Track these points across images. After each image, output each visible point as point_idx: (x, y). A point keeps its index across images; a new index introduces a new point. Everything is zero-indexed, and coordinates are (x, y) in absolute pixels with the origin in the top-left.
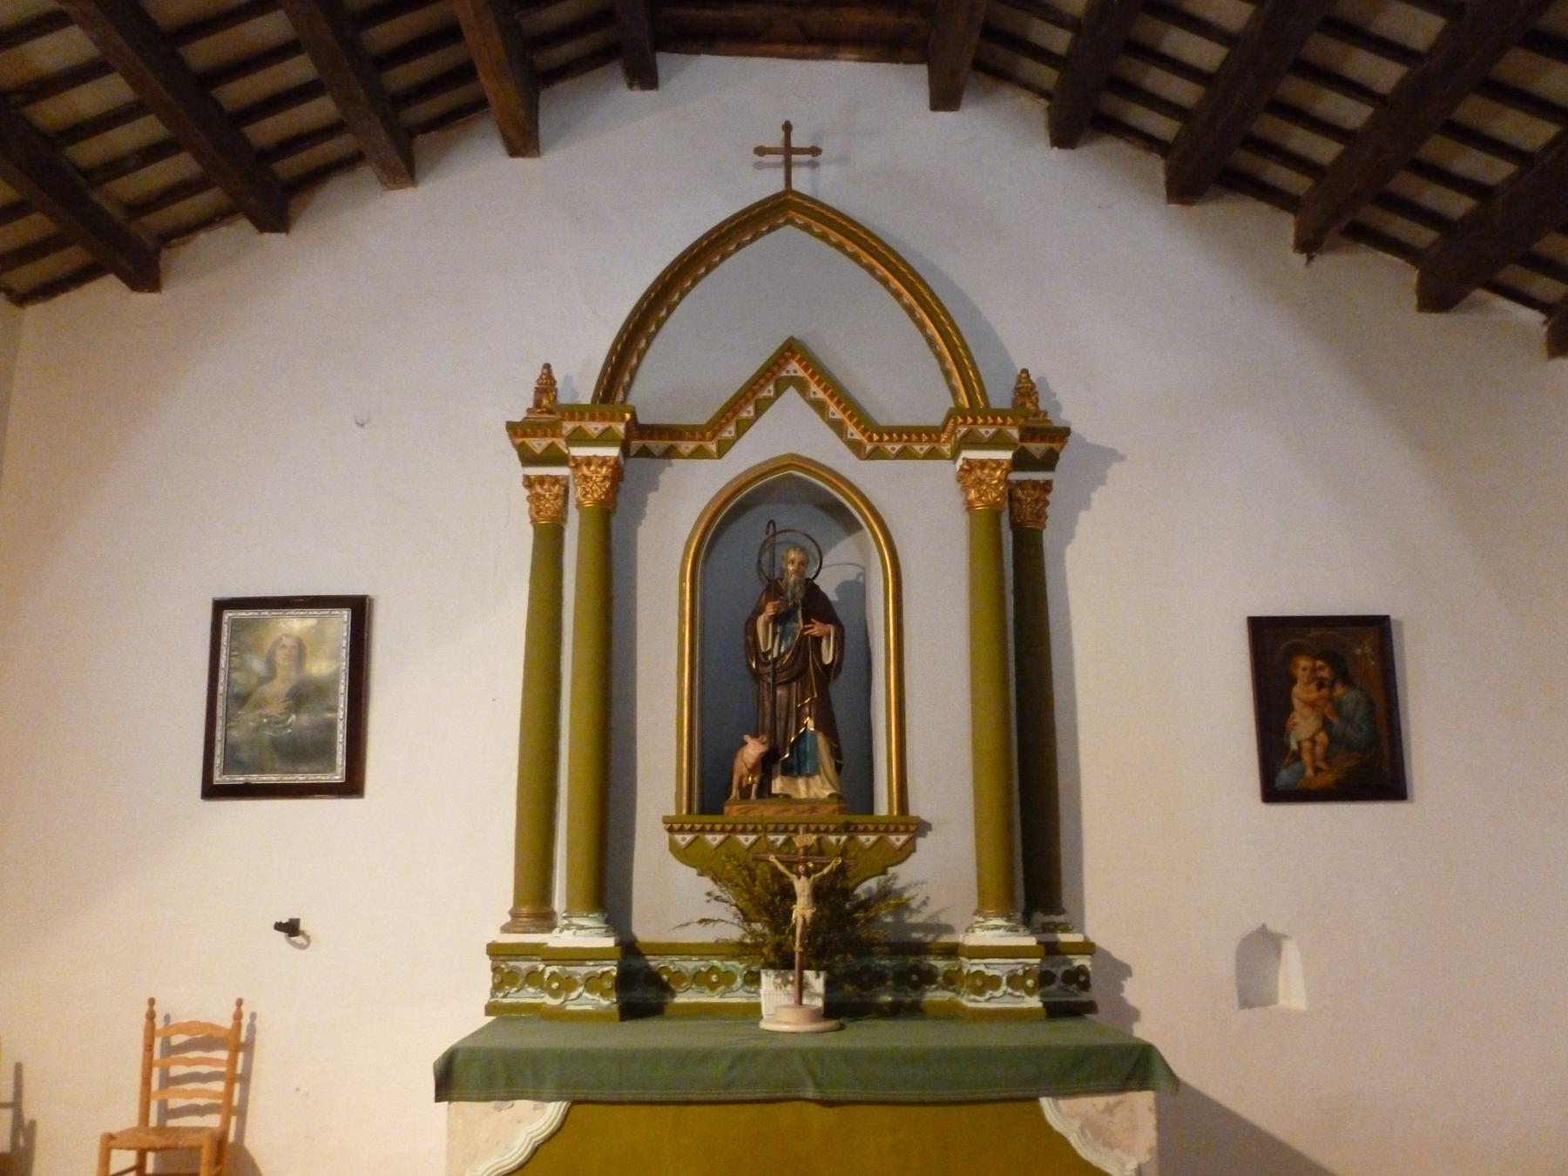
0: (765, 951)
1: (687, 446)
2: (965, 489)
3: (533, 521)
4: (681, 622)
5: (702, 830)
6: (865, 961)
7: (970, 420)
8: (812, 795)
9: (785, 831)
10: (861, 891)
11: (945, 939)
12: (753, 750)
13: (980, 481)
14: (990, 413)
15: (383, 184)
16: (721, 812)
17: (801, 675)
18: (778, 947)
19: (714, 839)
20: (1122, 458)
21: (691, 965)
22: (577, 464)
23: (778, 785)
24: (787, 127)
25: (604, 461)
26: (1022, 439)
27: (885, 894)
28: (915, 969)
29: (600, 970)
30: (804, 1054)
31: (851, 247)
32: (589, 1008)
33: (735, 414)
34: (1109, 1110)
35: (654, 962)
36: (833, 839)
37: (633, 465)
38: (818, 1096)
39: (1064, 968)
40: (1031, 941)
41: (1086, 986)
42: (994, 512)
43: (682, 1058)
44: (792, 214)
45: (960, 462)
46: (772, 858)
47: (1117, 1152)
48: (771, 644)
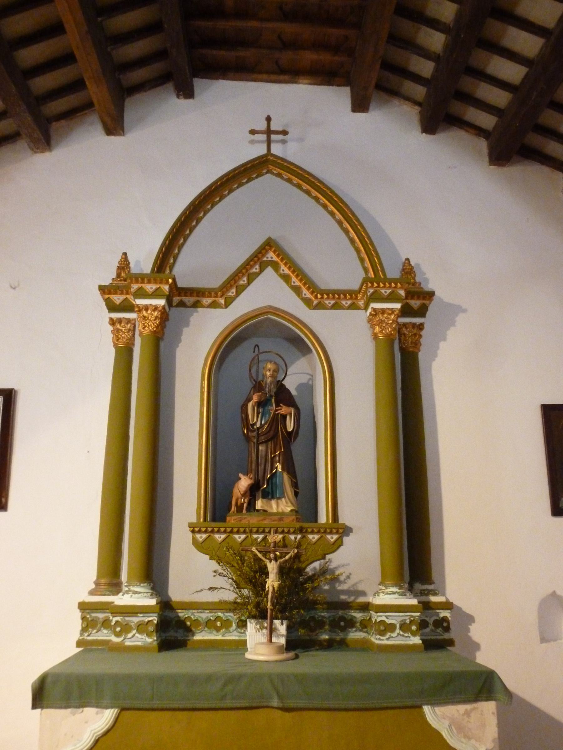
0: (249, 607)
1: (207, 301)
2: (373, 327)
3: (115, 345)
4: (202, 405)
5: (213, 531)
6: (313, 613)
7: (375, 285)
8: (280, 510)
9: (263, 532)
10: (309, 570)
11: (361, 600)
12: (244, 483)
13: (382, 322)
14: (386, 280)
15: (32, 149)
16: (224, 520)
17: (274, 437)
18: (257, 605)
19: (220, 537)
20: (465, 311)
21: (205, 615)
22: (140, 309)
23: (259, 504)
24: (269, 119)
25: (156, 308)
26: (407, 297)
27: (324, 571)
28: (342, 618)
29: (146, 620)
30: (270, 677)
31: (305, 186)
32: (139, 643)
33: (235, 282)
34: (467, 713)
35: (182, 614)
36: (292, 537)
37: (174, 313)
38: (281, 705)
39: (435, 618)
40: (414, 602)
41: (447, 629)
42: (390, 340)
43: (193, 680)
44: (271, 167)
45: (369, 310)
46: (254, 549)
47: (473, 742)
48: (257, 420)
